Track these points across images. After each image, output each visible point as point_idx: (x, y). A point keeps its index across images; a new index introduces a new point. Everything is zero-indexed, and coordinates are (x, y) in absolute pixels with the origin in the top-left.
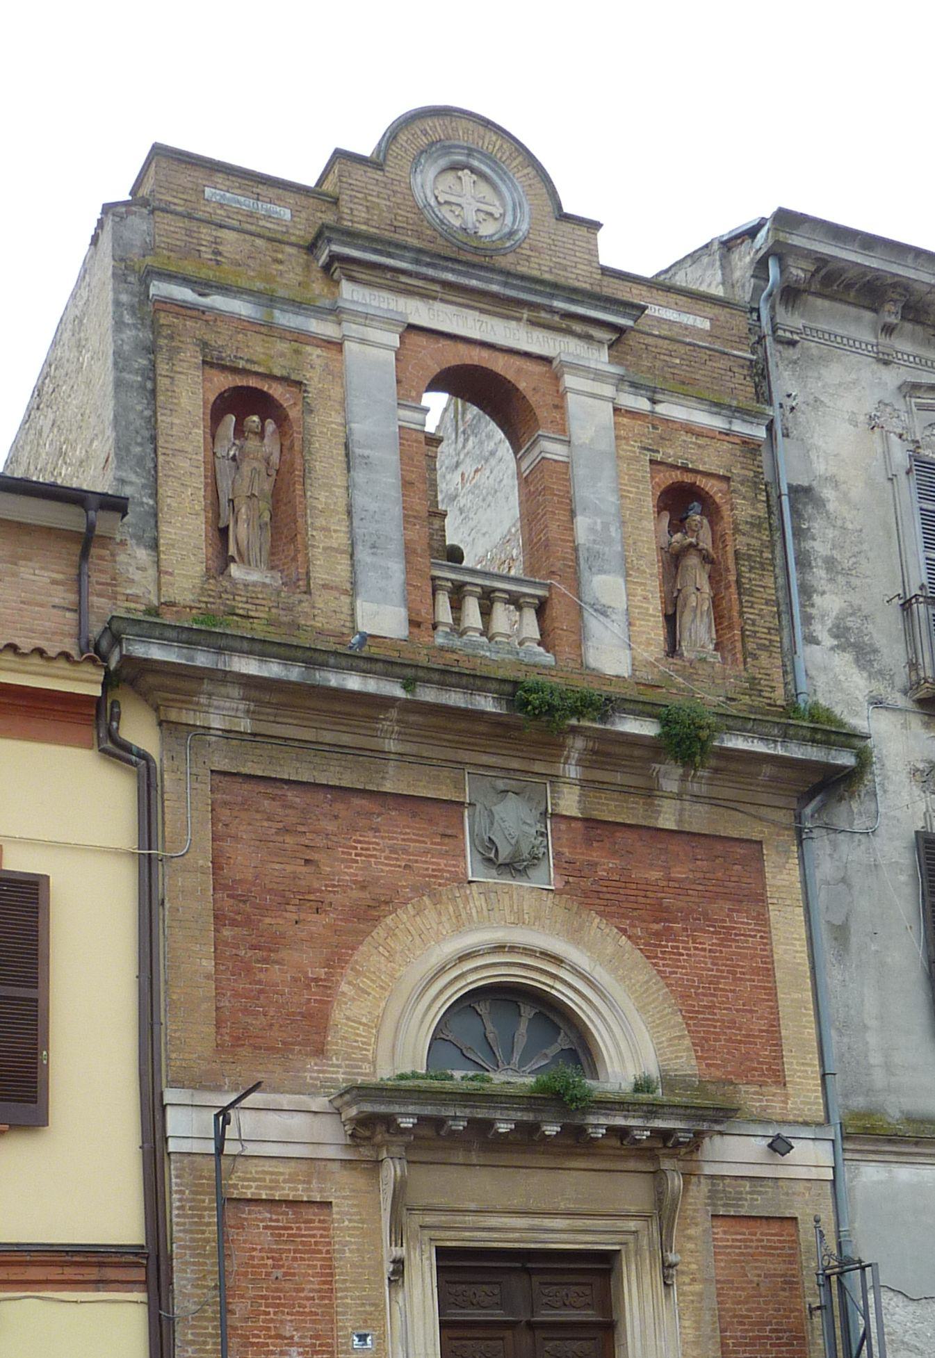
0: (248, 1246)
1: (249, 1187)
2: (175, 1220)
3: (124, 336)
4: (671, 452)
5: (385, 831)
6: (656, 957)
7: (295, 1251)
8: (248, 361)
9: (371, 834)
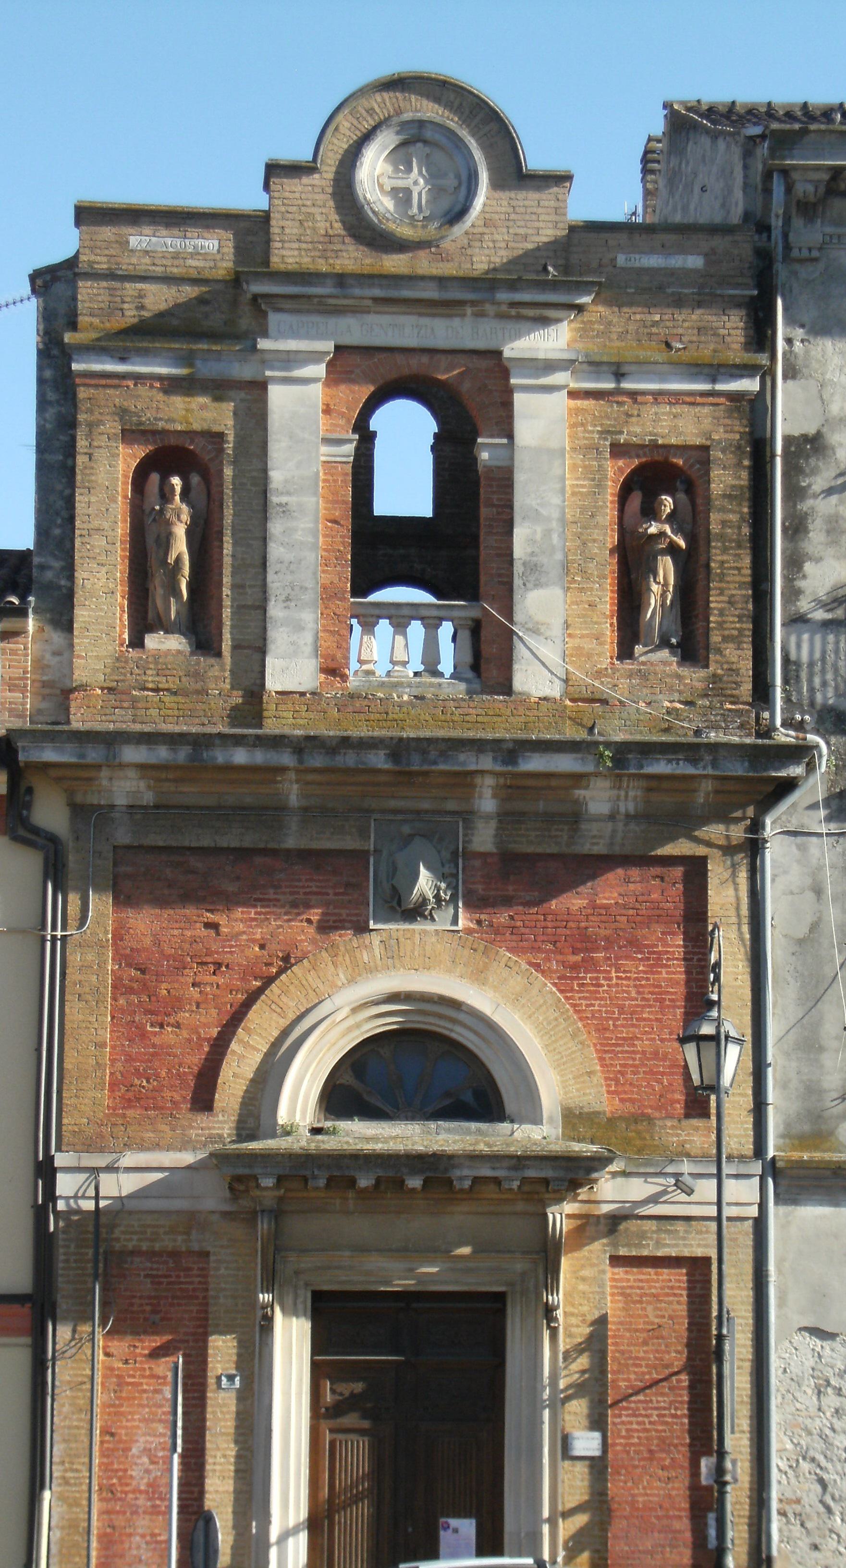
0: (128, 1293)
1: (131, 1240)
2: (60, 1272)
3: (47, 416)
4: (638, 430)
5: (286, 887)
6: (572, 990)
7: (173, 1297)
8: (167, 421)
9: (271, 891)
